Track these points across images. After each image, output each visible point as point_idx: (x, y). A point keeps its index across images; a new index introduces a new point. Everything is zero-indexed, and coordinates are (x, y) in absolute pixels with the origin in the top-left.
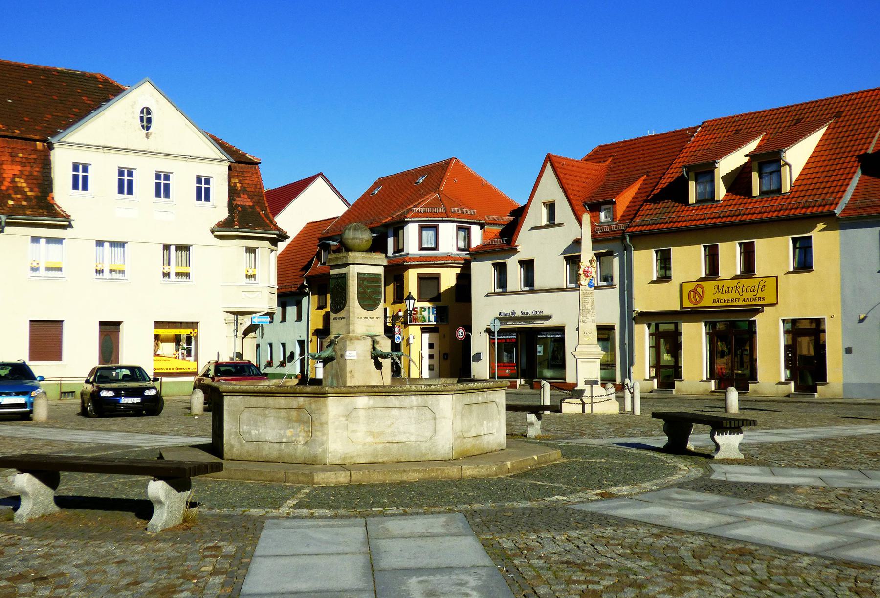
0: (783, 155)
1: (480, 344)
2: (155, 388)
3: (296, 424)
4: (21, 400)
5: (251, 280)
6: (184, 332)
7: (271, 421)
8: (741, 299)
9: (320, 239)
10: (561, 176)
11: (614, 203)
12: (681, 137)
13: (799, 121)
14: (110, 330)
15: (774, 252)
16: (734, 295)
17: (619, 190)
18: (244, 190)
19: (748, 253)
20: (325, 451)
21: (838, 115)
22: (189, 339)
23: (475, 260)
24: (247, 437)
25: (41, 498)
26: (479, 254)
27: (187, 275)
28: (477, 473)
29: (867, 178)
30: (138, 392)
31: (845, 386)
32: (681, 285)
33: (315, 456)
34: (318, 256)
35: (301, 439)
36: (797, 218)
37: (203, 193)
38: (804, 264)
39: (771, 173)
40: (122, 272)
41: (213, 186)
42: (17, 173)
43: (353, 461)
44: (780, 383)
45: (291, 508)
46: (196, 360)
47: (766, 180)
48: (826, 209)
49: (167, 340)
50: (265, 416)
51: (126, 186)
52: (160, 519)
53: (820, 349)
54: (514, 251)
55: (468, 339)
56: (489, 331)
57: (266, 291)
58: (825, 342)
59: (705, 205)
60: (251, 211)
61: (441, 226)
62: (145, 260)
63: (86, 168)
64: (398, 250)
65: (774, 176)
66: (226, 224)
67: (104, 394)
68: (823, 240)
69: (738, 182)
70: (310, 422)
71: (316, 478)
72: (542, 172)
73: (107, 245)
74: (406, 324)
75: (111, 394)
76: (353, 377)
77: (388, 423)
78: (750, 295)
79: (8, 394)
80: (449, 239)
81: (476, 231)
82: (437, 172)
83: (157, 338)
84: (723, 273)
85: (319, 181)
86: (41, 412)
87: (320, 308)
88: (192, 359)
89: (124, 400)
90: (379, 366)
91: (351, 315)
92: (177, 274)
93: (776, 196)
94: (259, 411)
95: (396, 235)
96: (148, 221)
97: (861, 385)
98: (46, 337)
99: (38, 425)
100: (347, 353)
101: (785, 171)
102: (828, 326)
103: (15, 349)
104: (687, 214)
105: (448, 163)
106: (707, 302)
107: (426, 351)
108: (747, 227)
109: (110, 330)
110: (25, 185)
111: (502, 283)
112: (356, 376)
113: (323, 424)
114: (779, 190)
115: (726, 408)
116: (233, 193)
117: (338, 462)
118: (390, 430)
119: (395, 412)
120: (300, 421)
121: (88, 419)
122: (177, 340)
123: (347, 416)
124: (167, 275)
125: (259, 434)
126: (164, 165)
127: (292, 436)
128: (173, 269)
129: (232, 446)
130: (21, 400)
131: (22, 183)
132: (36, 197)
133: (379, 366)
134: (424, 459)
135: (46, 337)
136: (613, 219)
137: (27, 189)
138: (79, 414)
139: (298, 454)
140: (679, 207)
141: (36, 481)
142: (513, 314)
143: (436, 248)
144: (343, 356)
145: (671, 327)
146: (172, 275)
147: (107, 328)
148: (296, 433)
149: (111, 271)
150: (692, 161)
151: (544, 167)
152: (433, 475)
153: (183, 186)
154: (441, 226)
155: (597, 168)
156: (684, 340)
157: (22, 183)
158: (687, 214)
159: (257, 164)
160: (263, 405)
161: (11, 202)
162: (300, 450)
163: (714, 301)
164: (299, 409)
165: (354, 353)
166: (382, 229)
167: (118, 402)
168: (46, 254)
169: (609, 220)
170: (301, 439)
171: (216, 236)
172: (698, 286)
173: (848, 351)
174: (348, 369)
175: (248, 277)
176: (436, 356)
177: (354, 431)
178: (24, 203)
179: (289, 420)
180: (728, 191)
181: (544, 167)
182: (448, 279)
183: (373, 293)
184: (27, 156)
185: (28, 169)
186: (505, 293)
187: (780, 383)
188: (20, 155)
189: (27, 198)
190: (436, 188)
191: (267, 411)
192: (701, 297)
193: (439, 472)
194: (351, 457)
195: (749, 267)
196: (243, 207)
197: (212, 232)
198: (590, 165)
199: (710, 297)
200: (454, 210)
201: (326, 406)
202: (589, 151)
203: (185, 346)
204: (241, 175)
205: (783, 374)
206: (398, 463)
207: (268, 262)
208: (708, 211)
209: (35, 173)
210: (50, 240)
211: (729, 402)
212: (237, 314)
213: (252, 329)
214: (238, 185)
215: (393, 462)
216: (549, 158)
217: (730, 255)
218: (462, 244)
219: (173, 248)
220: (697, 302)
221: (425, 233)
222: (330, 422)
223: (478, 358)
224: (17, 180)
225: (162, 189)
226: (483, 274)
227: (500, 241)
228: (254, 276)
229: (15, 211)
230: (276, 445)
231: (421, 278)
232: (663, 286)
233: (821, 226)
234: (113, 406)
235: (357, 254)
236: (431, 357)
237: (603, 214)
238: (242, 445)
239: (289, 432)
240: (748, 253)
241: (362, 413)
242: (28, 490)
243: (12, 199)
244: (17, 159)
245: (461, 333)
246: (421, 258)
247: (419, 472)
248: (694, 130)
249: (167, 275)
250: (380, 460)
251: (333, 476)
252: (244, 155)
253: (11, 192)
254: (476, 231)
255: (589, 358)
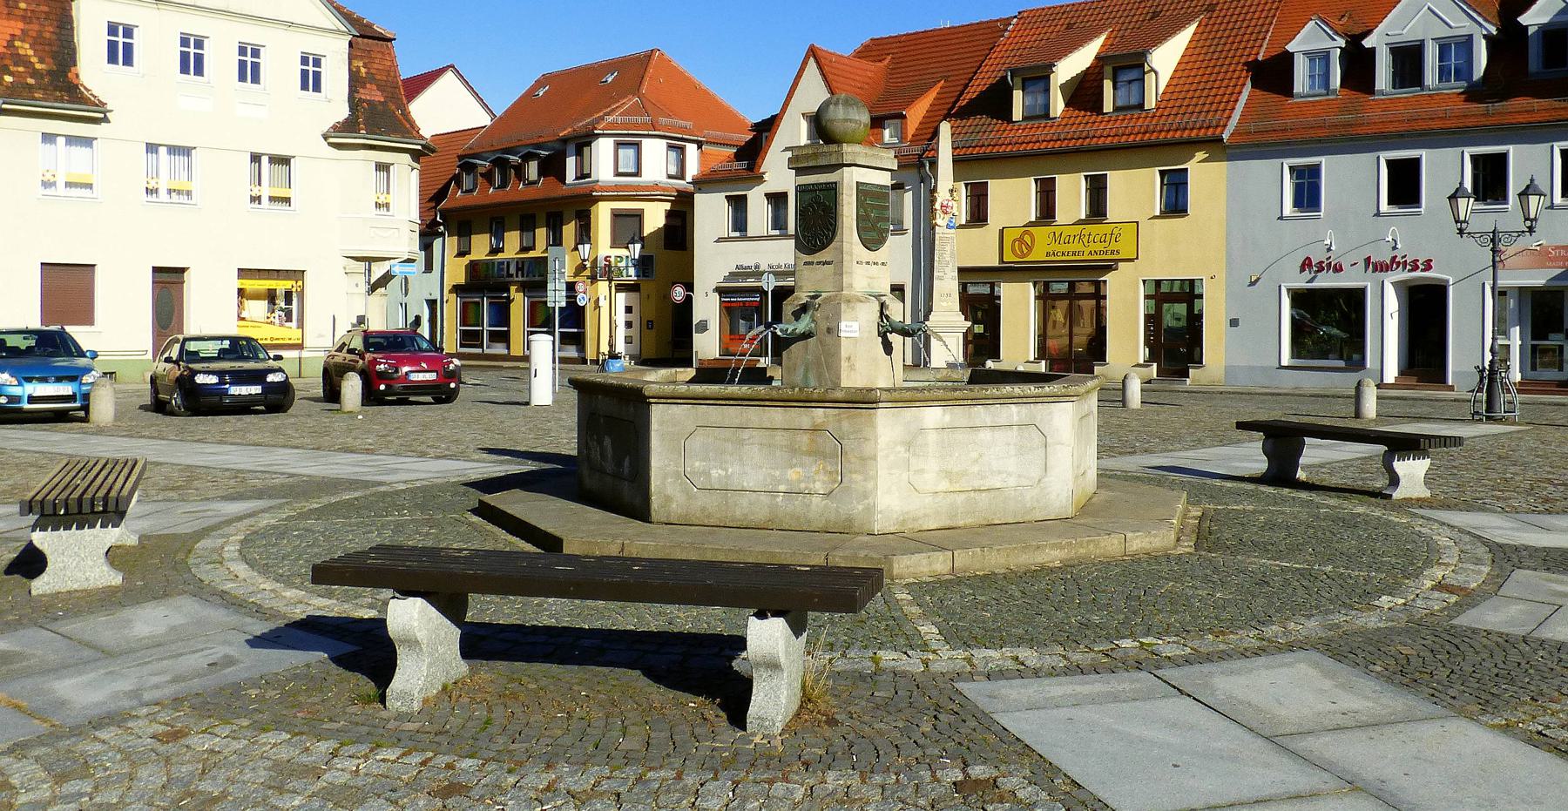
0: (1149, 58)
1: (706, 308)
2: (280, 370)
3: (807, 460)
4: (66, 389)
5: (383, 211)
6: (281, 286)
7: (754, 453)
8: (1085, 249)
9: (460, 157)
10: (831, 77)
11: (904, 117)
12: (990, 32)
13: (1155, 15)
14: (168, 280)
15: (1134, 190)
16: (1076, 246)
17: (910, 101)
18: (371, 78)
19: (1097, 190)
20: (870, 510)
21: (1211, 8)
22: (288, 296)
23: (700, 191)
24: (701, 481)
25: (441, 650)
26: (705, 182)
27: (287, 200)
28: (1148, 546)
29: (1258, 92)
30: (257, 377)
31: (1229, 370)
32: (1002, 232)
33: (850, 520)
34: (457, 179)
35: (819, 487)
36: (1168, 146)
37: (311, 80)
38: (1175, 205)
39: (1130, 82)
40: (189, 193)
41: (324, 70)
42: (18, 32)
43: (917, 526)
44: (1139, 365)
45: (914, 643)
46: (301, 325)
47: (1122, 92)
48: (1210, 132)
49: (256, 296)
50: (741, 442)
51: (192, 63)
52: (772, 702)
53: (1195, 320)
54: (760, 179)
55: (688, 301)
56: (721, 291)
57: (406, 227)
58: (1201, 311)
59: (1036, 123)
60: (377, 113)
61: (646, 142)
62: (222, 177)
63: (128, 32)
64: (582, 175)
65: (1135, 87)
66: (348, 127)
67: (201, 379)
68: (1203, 174)
69: (1084, 93)
70: (839, 456)
71: (896, 566)
72: (802, 70)
73: (163, 150)
74: (593, 279)
75: (213, 380)
76: (852, 367)
77: (974, 455)
78: (1100, 247)
79: (44, 380)
80: (656, 160)
81: (691, 149)
82: (634, 69)
83: (241, 292)
84: (1062, 216)
85: (449, 75)
86: (103, 407)
87: (461, 254)
88: (294, 324)
89: (235, 390)
90: (888, 348)
91: (846, 257)
92: (272, 199)
93: (1136, 113)
94: (728, 433)
95: (579, 153)
96: (223, 117)
97: (1252, 368)
98: (68, 287)
99: (100, 431)
100: (843, 325)
101: (1150, 79)
102: (1207, 290)
103: (20, 311)
104: (1010, 134)
105: (649, 55)
106: (1038, 255)
107: (621, 317)
108: (1099, 157)
109: (168, 280)
110: (31, 52)
111: (740, 223)
112: (857, 366)
113: (867, 460)
114: (1141, 106)
115: (1358, 415)
116: (355, 81)
117: (892, 530)
118: (976, 469)
119: (985, 435)
120: (816, 453)
121: (168, 419)
122: (271, 296)
123: (909, 445)
124: (256, 199)
125: (727, 477)
126: (252, 34)
127: (800, 481)
128: (265, 191)
129: (668, 499)
130: (66, 389)
131: (25, 49)
132: (49, 73)
133: (888, 348)
134: (1027, 518)
135: (68, 287)
136: (902, 139)
137: (34, 60)
138: (143, 408)
139: (811, 515)
140: (997, 124)
141: (433, 612)
142: (757, 267)
143: (637, 174)
144: (832, 331)
145: (986, 290)
146: (265, 200)
147: (165, 277)
148: (811, 477)
149: (170, 192)
150: (1015, 62)
151: (805, 63)
152: (1082, 551)
153: (281, 67)
154: (646, 142)
155: (872, 69)
156: (1004, 304)
157: (25, 49)
158: (1010, 134)
159: (390, 40)
160: (736, 422)
161: (8, 79)
162: (817, 508)
163: (1048, 254)
164: (815, 430)
165: (855, 325)
166: (557, 146)
167: (225, 393)
168: (68, 161)
169: (895, 140)
170: (819, 487)
171: (330, 144)
172: (1026, 232)
173: (1234, 323)
174: (844, 354)
175: (378, 205)
176: (636, 324)
177: (922, 471)
178: (31, 81)
179: (793, 450)
180: (1067, 105)
181: (805, 63)
182: (655, 217)
183: (879, 219)
184: (33, 7)
185: (36, 27)
186: (744, 237)
187: (1139, 365)
188: (23, 5)
189: (34, 73)
190: (636, 90)
191: (746, 434)
192: (1030, 249)
193: (1091, 546)
194: (915, 519)
195: (1097, 208)
196: (369, 103)
197: (325, 137)
198: (864, 64)
199: (1043, 248)
200: (663, 120)
201: (873, 426)
202: (857, 46)
203: (283, 305)
204: (367, 57)
205: (1142, 353)
206: (988, 531)
207: (407, 183)
208: (1041, 132)
209: (47, 35)
210: (72, 140)
211: (1129, 393)
212: (370, 260)
213: (386, 279)
214: (363, 70)
215: (981, 526)
216: (813, 52)
217: (1072, 191)
218: (673, 170)
219: (265, 160)
220: (1024, 255)
221: (621, 151)
222: (880, 455)
223: (703, 327)
224: (17, 43)
225: (249, 70)
226: (711, 212)
227: (736, 165)
228: (387, 206)
229: (13, 92)
230: (764, 498)
231: (617, 215)
232: (974, 232)
233: (1200, 155)
234: (217, 399)
235: (858, 148)
236: (629, 325)
237: (887, 132)
238: (690, 496)
239: (792, 474)
240: (1097, 190)
241: (932, 437)
242: (421, 635)
243: (11, 74)
244: (16, 12)
245: (678, 293)
246: (617, 187)
247: (1062, 548)
248: (1007, 22)
249: (256, 199)
250: (961, 523)
251: (925, 562)
252: (369, 26)
253: (7, 62)
254: (691, 149)
255: (951, 330)
